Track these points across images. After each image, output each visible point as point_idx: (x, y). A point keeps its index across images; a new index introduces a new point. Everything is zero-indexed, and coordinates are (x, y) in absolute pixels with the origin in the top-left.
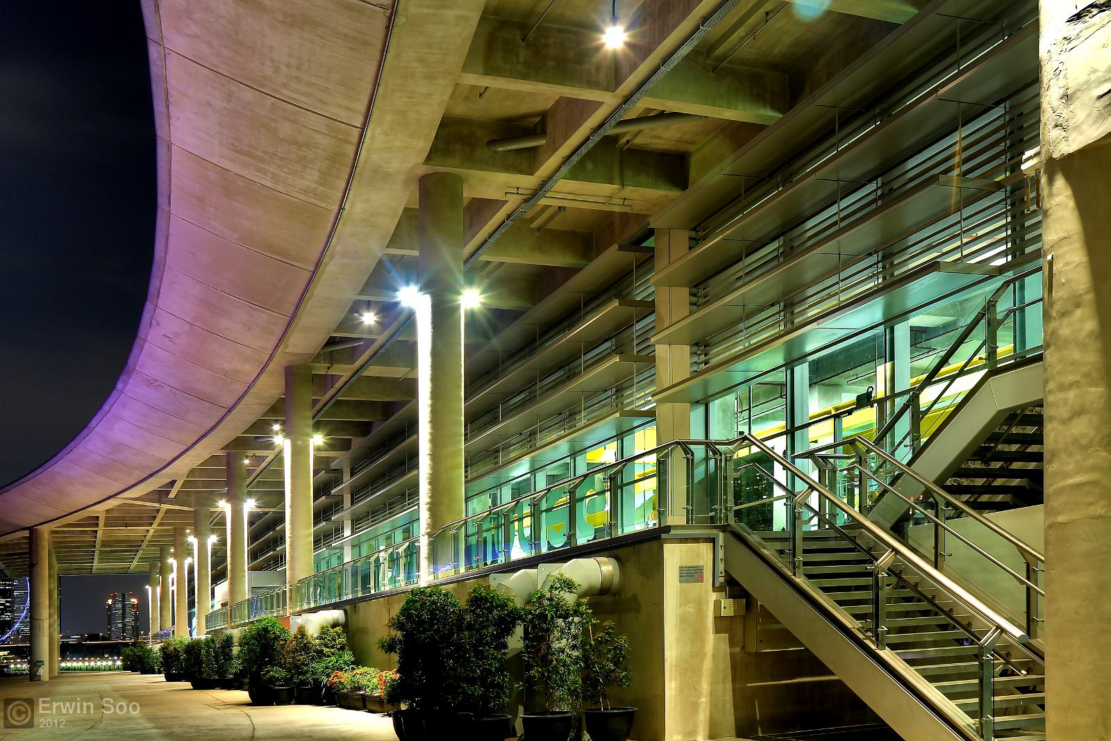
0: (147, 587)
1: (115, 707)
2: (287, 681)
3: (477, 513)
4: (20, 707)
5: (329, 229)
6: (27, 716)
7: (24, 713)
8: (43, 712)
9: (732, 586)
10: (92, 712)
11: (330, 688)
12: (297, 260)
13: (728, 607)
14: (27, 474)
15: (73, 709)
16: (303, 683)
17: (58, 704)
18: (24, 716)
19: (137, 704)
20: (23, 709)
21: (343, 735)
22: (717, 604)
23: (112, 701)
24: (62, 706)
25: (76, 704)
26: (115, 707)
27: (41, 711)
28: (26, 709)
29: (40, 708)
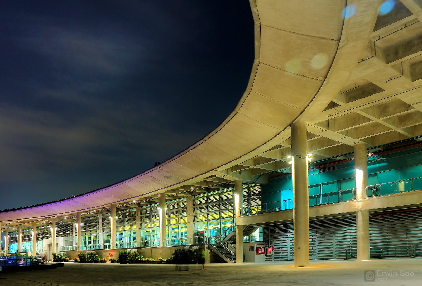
0: (5, 237)
1: (405, 274)
2: (131, 260)
3: (89, 232)
4: (369, 274)
5: (279, 70)
6: (373, 277)
7: (371, 276)
8: (379, 275)
9: (210, 249)
10: (397, 275)
11: (140, 261)
12: (400, 69)
13: (210, 251)
14: (173, 157)
15: (389, 275)
16: (134, 260)
17: (384, 272)
18: (371, 277)
19: (407, 272)
20: (371, 275)
21: (280, 272)
22: (209, 251)
24: (386, 274)
25: (391, 272)
26: (410, 274)
27: (378, 275)
28: (372, 274)
29: (378, 274)
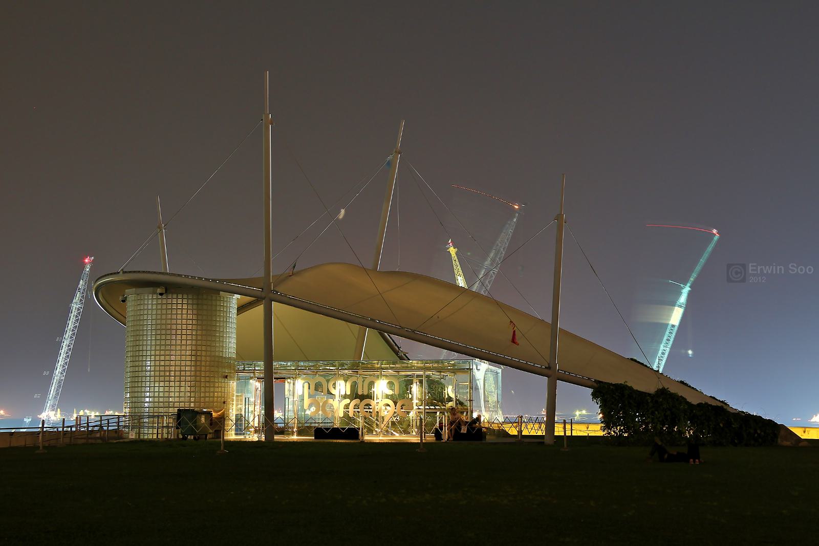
23: (795, 265)
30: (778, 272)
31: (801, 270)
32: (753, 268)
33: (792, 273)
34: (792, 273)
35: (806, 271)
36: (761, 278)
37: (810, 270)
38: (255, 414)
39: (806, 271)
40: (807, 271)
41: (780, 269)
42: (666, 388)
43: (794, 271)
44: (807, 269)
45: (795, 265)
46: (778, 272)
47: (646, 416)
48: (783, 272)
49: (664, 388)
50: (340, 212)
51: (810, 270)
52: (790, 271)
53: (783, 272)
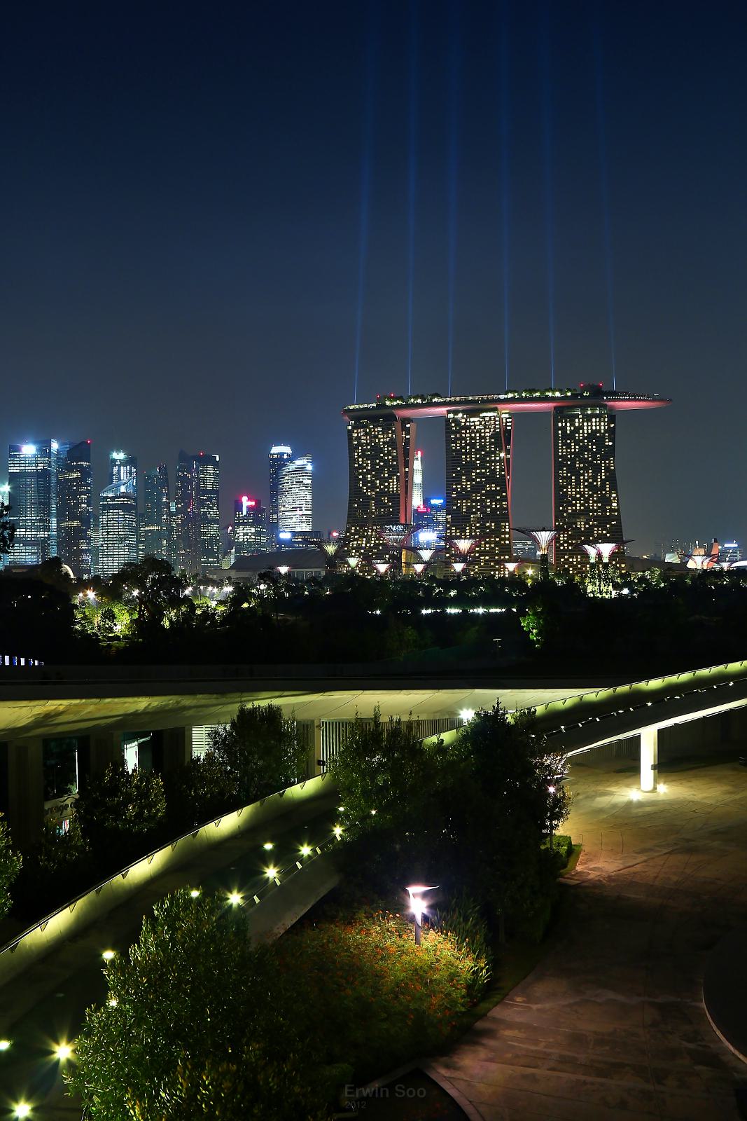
23: (404, 1087)
29: (346, 1093)
30: (382, 1096)
31: (411, 1093)
32: (350, 1090)
33: (401, 1085)
34: (400, 1096)
35: (416, 1093)
36: (360, 1103)
37: (422, 1093)
38: (696, 553)
39: (416, 1093)
40: (418, 1094)
41: (384, 1092)
42: (491, 712)
43: (402, 1093)
44: (414, 1094)
45: (404, 1087)
46: (382, 1096)
47: (220, 1034)
48: (387, 1096)
49: (486, 715)
50: (427, 615)
51: (422, 1093)
52: (397, 1095)
53: (387, 1096)
